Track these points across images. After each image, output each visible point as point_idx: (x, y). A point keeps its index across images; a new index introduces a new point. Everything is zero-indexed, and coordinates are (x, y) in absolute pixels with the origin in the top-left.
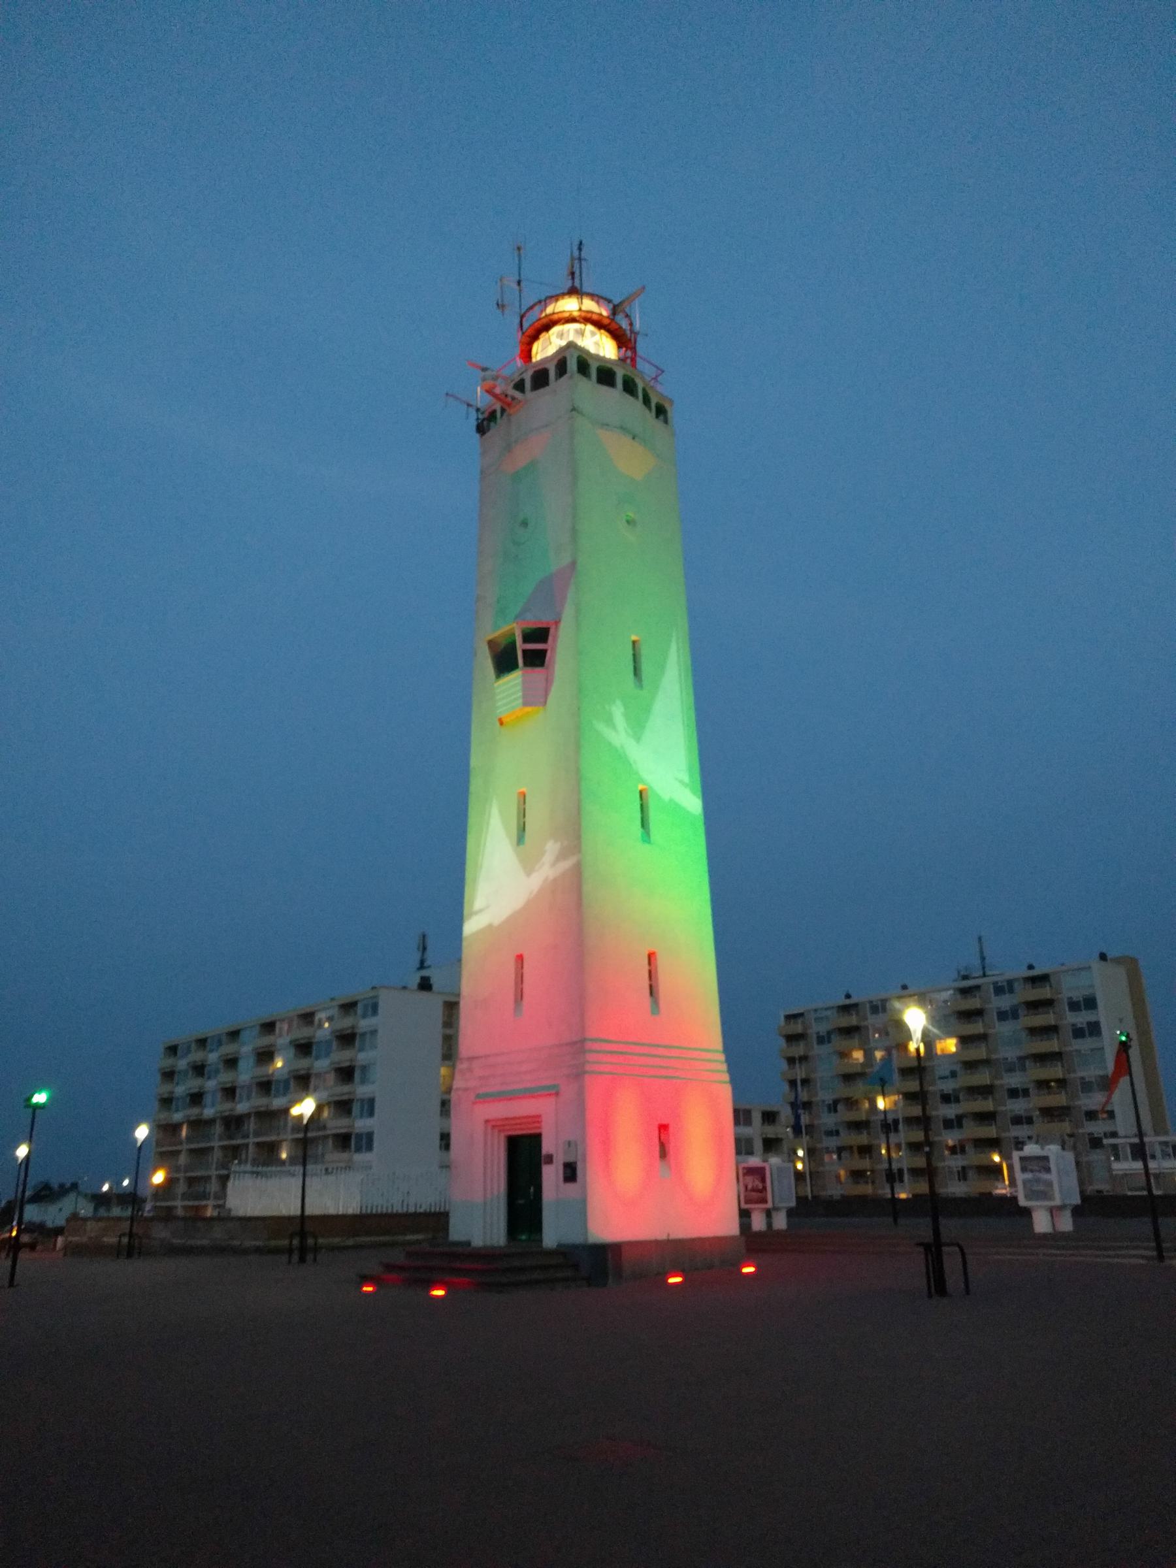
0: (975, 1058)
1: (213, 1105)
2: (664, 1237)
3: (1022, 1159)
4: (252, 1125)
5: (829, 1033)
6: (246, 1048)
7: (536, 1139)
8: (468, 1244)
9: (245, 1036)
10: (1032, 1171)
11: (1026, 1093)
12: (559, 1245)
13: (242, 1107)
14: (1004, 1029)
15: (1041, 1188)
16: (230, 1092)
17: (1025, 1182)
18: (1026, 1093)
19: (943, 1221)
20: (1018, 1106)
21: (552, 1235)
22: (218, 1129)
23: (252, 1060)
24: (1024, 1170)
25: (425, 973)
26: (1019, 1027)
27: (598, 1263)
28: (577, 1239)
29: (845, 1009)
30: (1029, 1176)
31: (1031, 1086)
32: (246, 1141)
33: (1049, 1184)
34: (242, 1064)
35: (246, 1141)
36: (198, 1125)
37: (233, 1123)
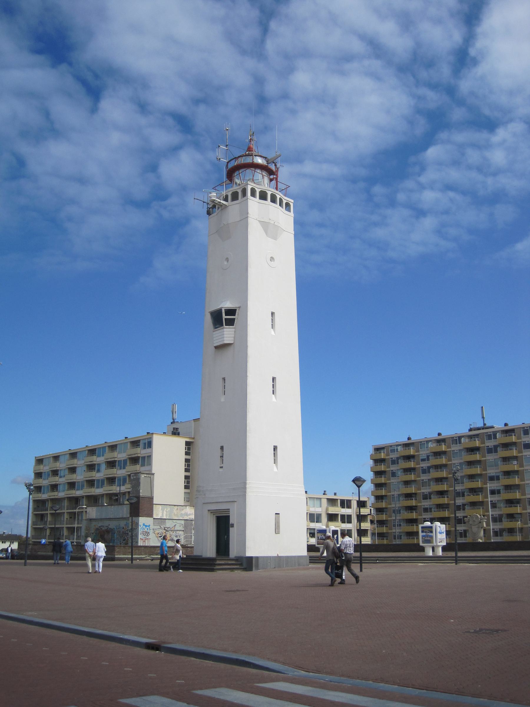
0: (474, 473)
1: (64, 491)
2: (276, 555)
3: (422, 527)
4: (49, 505)
5: (398, 458)
6: (80, 463)
7: (228, 518)
8: (201, 556)
9: (62, 459)
10: (426, 532)
11: (499, 492)
12: (236, 557)
13: (78, 493)
14: (490, 457)
15: (428, 539)
16: (72, 485)
17: (423, 536)
18: (499, 492)
19: (363, 553)
20: (426, 504)
21: (234, 552)
22: (66, 503)
23: (85, 468)
24: (422, 532)
25: (175, 426)
26: (498, 457)
27: (248, 564)
28: (241, 555)
29: (406, 445)
30: (424, 534)
31: (501, 488)
32: (47, 512)
33: (432, 537)
34: (78, 470)
35: (47, 512)
36: (55, 501)
37: (75, 501)
